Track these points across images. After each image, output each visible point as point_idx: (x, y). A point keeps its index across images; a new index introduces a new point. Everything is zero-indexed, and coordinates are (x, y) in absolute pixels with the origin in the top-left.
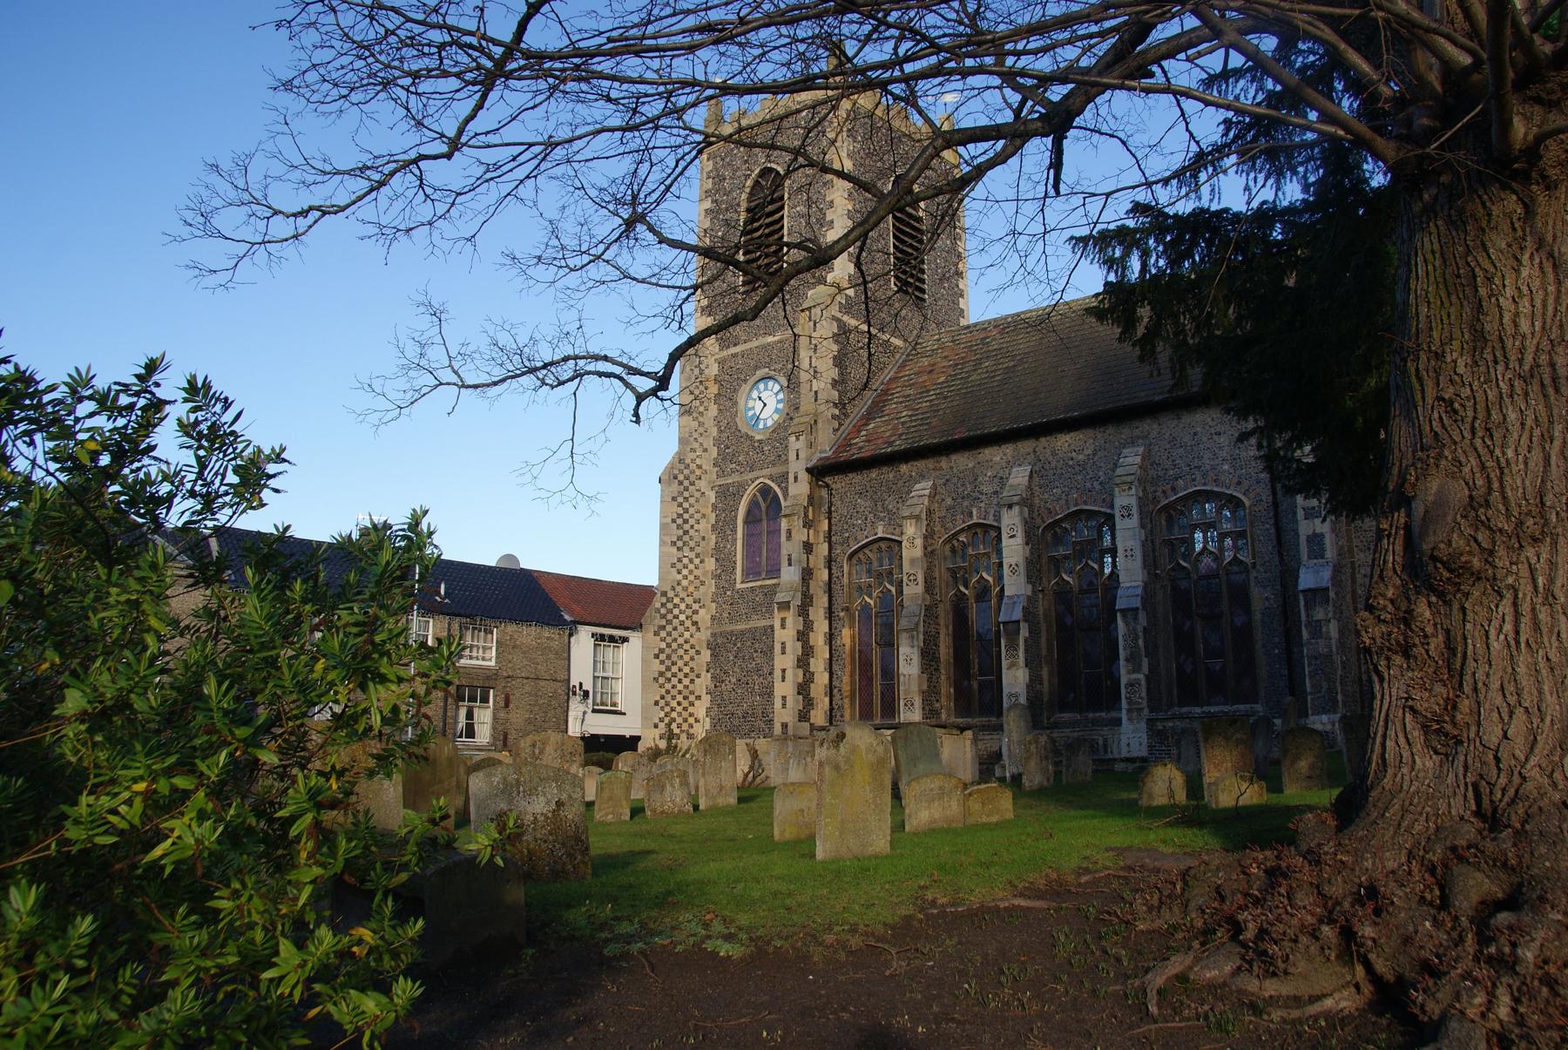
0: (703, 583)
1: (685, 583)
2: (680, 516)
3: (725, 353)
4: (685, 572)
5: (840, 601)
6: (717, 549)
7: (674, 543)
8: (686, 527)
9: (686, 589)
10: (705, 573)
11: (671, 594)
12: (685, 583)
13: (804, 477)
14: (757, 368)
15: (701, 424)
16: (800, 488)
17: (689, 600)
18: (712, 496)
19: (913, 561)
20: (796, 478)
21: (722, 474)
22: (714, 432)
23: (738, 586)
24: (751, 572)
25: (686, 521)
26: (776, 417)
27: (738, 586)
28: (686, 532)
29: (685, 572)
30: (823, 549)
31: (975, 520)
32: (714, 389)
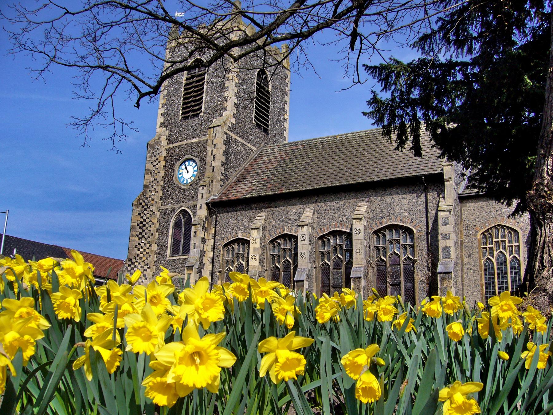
0: (150, 256)
1: (141, 255)
2: (141, 223)
3: (171, 146)
4: (142, 250)
5: (217, 268)
6: (159, 240)
7: (137, 236)
8: (144, 228)
9: (141, 258)
10: (151, 251)
11: (134, 260)
12: (141, 255)
13: (205, 207)
14: (185, 154)
15: (156, 179)
16: (203, 213)
17: (143, 264)
18: (158, 214)
19: (255, 250)
20: (200, 207)
21: (164, 204)
22: (162, 183)
23: (168, 258)
24: (175, 252)
25: (144, 226)
26: (193, 178)
27: (168, 258)
28: (144, 231)
29: (142, 250)
30: (211, 242)
31: (286, 232)
32: (163, 163)
